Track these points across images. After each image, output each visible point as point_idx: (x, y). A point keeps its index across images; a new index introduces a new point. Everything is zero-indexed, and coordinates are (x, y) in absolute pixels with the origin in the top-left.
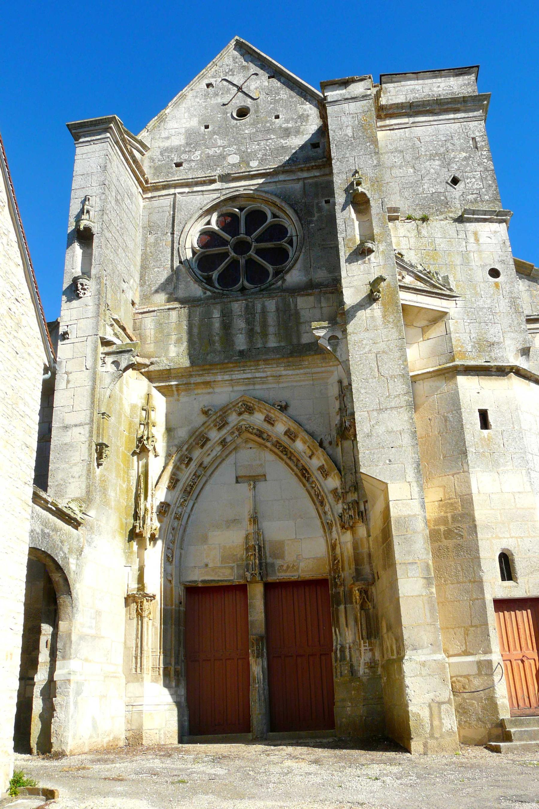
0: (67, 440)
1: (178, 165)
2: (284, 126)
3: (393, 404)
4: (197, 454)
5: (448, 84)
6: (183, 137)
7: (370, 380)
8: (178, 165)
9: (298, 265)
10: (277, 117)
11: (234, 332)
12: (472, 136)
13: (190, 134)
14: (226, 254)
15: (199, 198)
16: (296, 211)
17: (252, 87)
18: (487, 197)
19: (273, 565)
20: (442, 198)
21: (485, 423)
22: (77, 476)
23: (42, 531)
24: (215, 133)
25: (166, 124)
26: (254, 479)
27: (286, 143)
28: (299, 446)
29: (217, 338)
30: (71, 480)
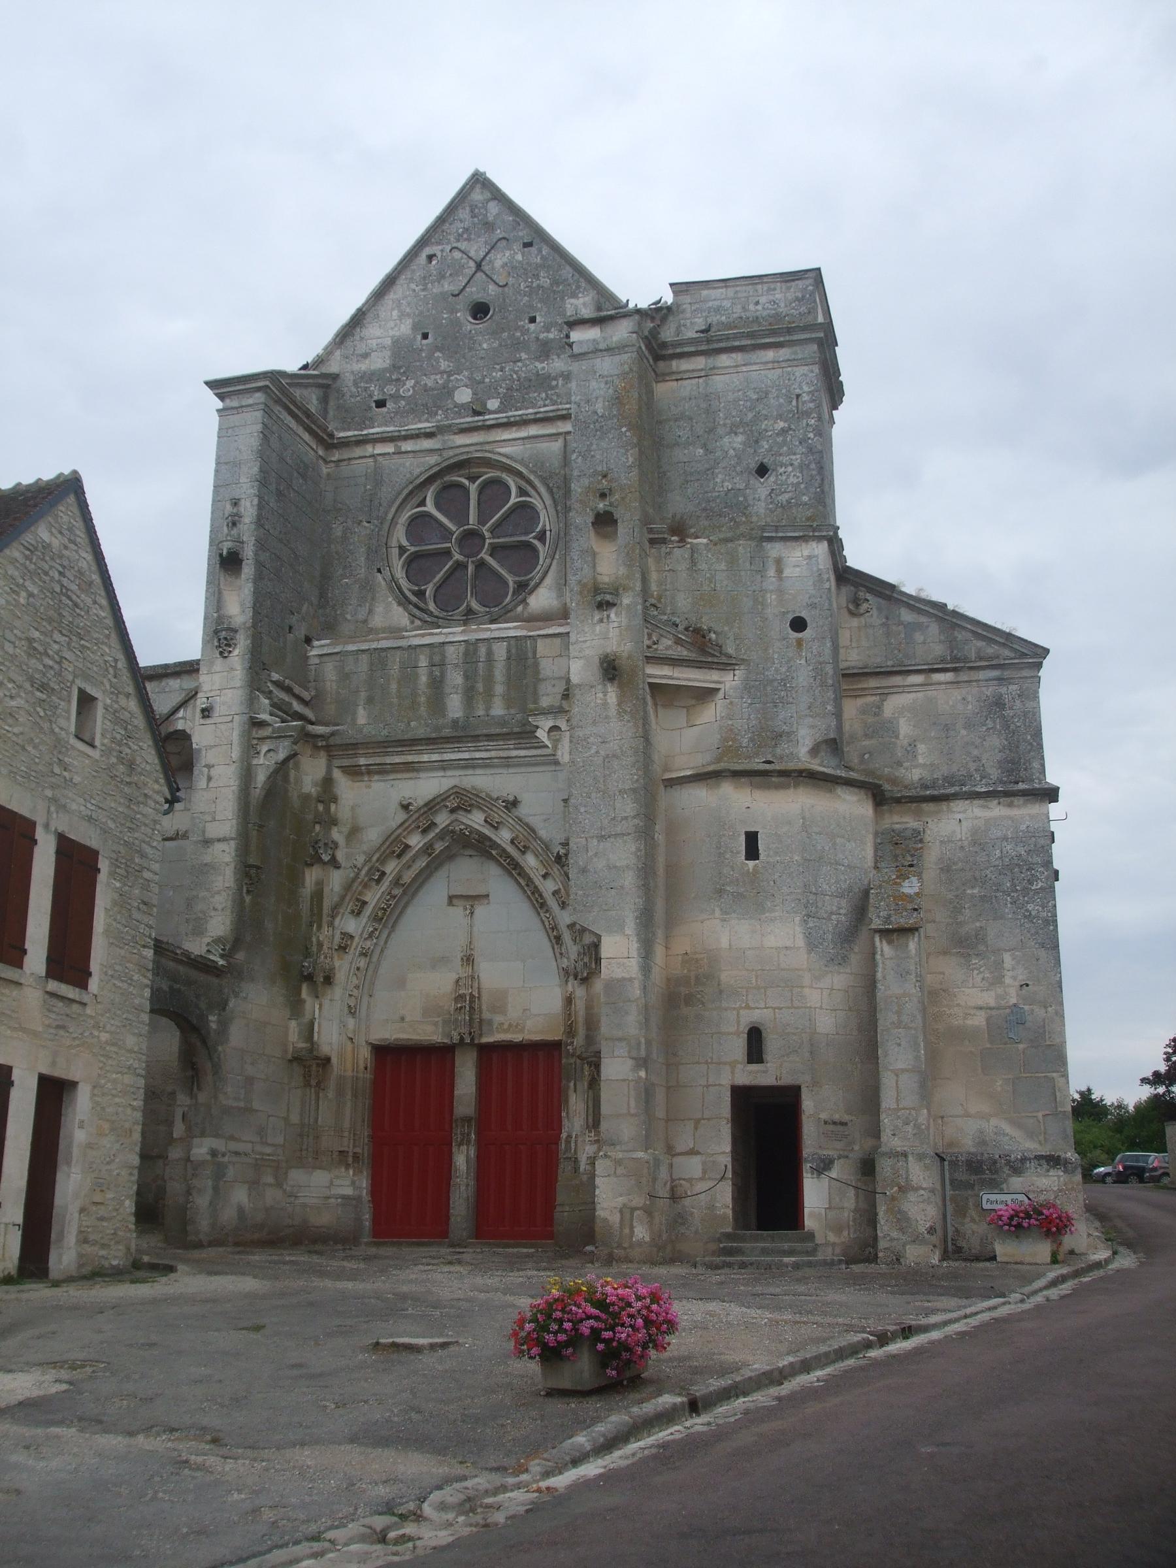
0: (207, 859)
1: (381, 404)
2: (542, 336)
3: (618, 830)
4: (391, 867)
5: (771, 298)
6: (389, 353)
7: (593, 795)
8: (381, 404)
9: (548, 580)
10: (533, 320)
11: (447, 690)
12: (798, 391)
13: (400, 349)
14: (447, 553)
15: (408, 462)
16: (550, 491)
17: (498, 263)
18: (805, 498)
19: (490, 1022)
20: (741, 499)
21: (752, 851)
22: (220, 907)
23: (171, 988)
24: (438, 349)
25: (363, 330)
26: (473, 900)
27: (543, 368)
28: (530, 862)
29: (423, 699)
30: (213, 913)
